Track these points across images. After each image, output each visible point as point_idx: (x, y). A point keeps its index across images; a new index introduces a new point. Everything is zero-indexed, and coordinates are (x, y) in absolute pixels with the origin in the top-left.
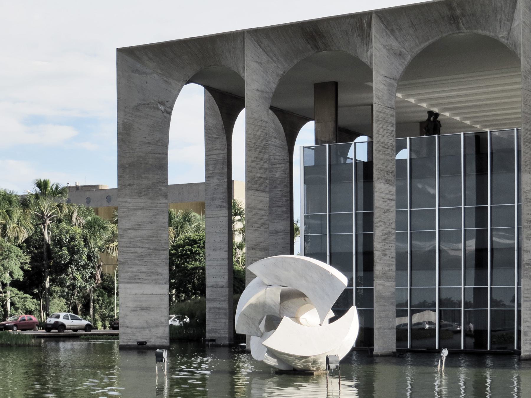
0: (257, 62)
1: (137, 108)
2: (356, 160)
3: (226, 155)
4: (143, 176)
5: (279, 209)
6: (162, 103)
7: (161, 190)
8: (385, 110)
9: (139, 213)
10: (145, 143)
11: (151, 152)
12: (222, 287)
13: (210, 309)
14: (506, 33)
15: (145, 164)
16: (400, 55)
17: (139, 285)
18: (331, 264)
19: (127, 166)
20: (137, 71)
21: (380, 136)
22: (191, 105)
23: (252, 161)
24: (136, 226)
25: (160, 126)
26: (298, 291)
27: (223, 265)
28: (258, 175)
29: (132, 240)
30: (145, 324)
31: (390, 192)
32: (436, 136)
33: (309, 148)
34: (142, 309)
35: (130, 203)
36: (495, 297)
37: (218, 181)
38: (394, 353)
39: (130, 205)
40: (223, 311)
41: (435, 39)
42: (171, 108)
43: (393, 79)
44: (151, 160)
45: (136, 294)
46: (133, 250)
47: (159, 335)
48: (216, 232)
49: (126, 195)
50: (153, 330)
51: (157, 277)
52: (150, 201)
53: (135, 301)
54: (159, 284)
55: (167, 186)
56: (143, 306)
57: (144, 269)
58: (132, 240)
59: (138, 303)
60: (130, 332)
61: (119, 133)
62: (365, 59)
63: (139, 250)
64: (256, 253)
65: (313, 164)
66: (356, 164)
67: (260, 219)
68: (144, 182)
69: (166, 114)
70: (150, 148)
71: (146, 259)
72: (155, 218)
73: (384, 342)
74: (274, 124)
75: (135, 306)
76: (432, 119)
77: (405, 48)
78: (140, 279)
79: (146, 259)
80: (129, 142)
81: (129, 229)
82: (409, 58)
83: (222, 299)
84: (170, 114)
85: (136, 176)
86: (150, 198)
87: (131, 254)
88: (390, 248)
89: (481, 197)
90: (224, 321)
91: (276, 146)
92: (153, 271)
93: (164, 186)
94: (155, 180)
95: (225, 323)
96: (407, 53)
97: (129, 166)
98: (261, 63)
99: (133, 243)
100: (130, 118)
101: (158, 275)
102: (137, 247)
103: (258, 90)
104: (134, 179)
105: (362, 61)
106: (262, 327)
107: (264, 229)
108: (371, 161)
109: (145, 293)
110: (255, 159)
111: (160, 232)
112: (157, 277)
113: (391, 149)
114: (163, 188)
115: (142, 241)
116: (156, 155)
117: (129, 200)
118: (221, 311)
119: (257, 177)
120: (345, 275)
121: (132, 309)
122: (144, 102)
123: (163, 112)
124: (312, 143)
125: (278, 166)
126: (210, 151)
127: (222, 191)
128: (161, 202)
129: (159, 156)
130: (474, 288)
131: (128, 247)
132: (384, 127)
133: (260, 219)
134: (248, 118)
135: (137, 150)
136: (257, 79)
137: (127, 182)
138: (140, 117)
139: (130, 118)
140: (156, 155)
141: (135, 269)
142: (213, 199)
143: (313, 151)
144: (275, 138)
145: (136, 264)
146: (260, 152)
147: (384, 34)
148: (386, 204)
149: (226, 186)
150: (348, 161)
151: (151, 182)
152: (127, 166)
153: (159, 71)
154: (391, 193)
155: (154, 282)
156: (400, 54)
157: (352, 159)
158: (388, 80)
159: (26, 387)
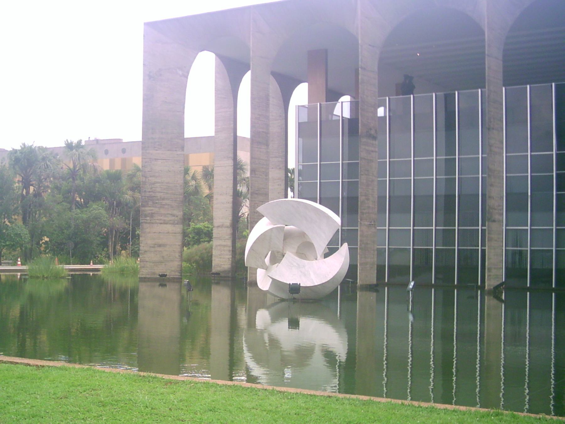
2: (342, 117)
13: (216, 246)
18: (320, 203)
22: (205, 68)
32: (412, 96)
33: (303, 106)
36: (438, 194)
38: (218, 283)
42: (188, 73)
55: (184, 139)
62: (308, 240)
65: (307, 121)
66: (343, 120)
73: (365, 276)
74: (274, 87)
76: (407, 82)
84: (187, 77)
89: (450, 149)
106: (267, 260)
108: (354, 117)
118: (225, 248)
120: (294, 89)
124: (305, 102)
130: (446, 159)
134: (253, 80)
143: (306, 110)
149: (232, 139)
150: (334, 118)
157: (339, 116)
159: (205, 169)
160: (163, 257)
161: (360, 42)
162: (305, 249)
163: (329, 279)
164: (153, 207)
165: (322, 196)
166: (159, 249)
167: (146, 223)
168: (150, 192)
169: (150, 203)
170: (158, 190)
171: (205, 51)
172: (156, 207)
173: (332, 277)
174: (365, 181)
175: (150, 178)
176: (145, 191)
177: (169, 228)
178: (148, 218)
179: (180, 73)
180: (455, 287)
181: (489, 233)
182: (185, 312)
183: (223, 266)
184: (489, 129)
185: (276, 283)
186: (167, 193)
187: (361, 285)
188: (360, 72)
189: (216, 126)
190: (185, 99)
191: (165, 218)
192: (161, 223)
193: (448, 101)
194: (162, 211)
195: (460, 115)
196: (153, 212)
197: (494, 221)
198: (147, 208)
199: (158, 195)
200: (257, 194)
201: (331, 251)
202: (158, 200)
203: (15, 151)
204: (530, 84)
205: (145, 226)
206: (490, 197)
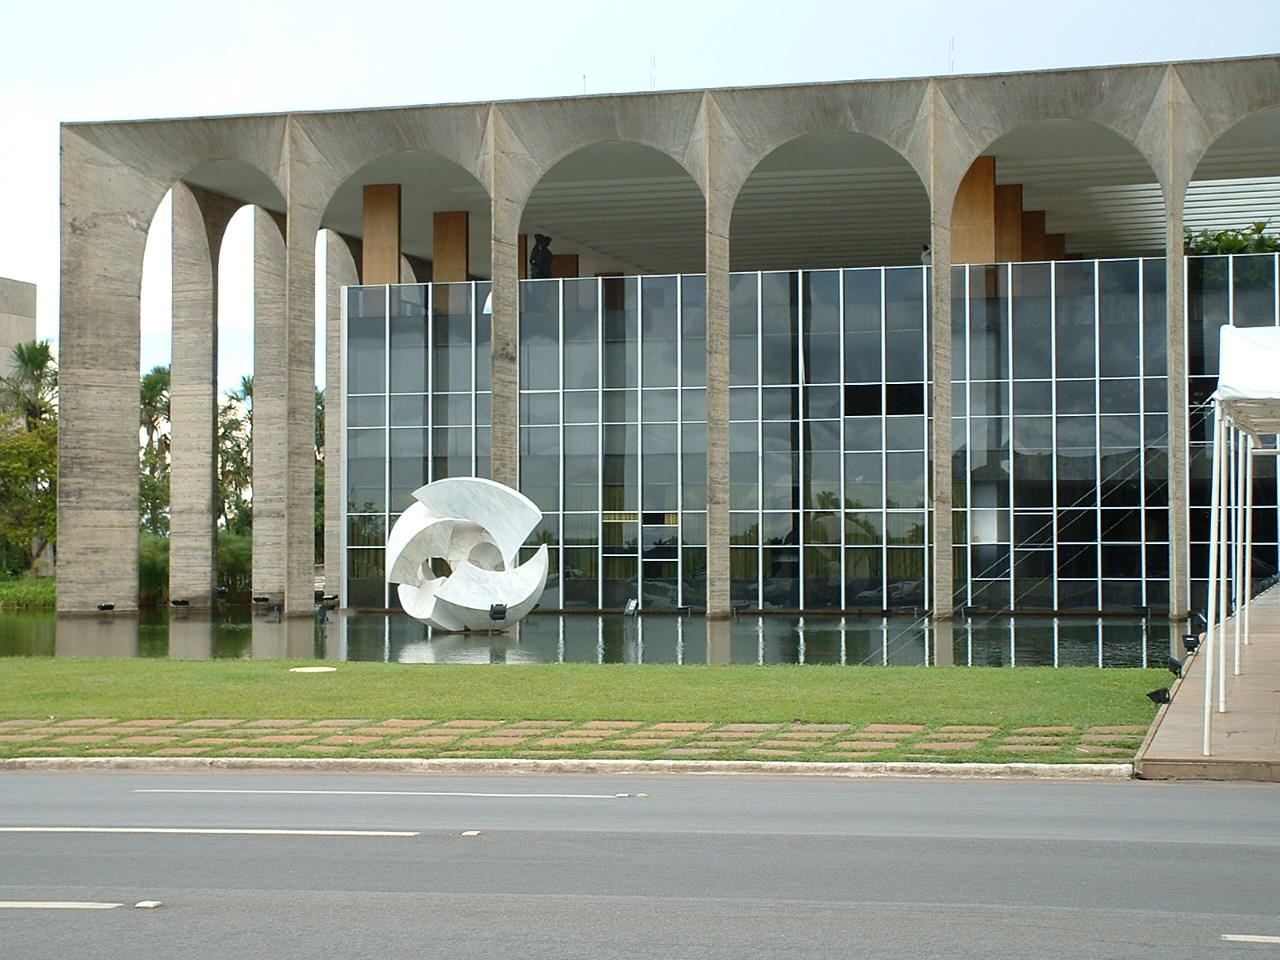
3: (211, 292)
5: (272, 379)
6: (134, 215)
12: (202, 512)
13: (178, 549)
14: (682, 147)
26: (476, 524)
27: (203, 476)
37: (195, 335)
40: (202, 553)
48: (190, 420)
60: (75, 590)
69: (138, 232)
75: (85, 546)
77: (534, 158)
83: (201, 532)
84: (146, 231)
90: (202, 569)
91: (269, 273)
93: (133, 349)
95: (205, 573)
105: (466, 171)
125: (272, 306)
126: (180, 284)
127: (202, 352)
135: (92, 289)
136: (307, 178)
140: (122, 298)
142: (187, 364)
144: (268, 259)
160: (102, 573)
161: (492, 195)
162: (486, 553)
163: (524, 599)
164: (82, 477)
165: (393, 456)
166: (92, 557)
167: (69, 508)
168: (75, 448)
169: (76, 470)
170: (92, 444)
171: (791, 530)
172: (87, 477)
173: (529, 595)
174: (500, 435)
175: (75, 423)
176: (66, 448)
177: (113, 516)
178: (73, 499)
179: (134, 222)
180: (1010, 614)
181: (711, 523)
182: (205, 379)
183: (193, 588)
184: (710, 353)
185: (442, 605)
186: (109, 451)
187: (289, 612)
188: (493, 246)
189: (173, 316)
190: (141, 271)
191: (106, 499)
192: (98, 509)
193: (529, 453)
194: (100, 485)
195: (393, 448)
196: (82, 486)
197: (718, 503)
198: (69, 480)
199: (92, 454)
200: (296, 454)
201: (525, 555)
202: (91, 463)
203: (435, 653)
204: (802, 268)
205: (68, 513)
206: (711, 463)
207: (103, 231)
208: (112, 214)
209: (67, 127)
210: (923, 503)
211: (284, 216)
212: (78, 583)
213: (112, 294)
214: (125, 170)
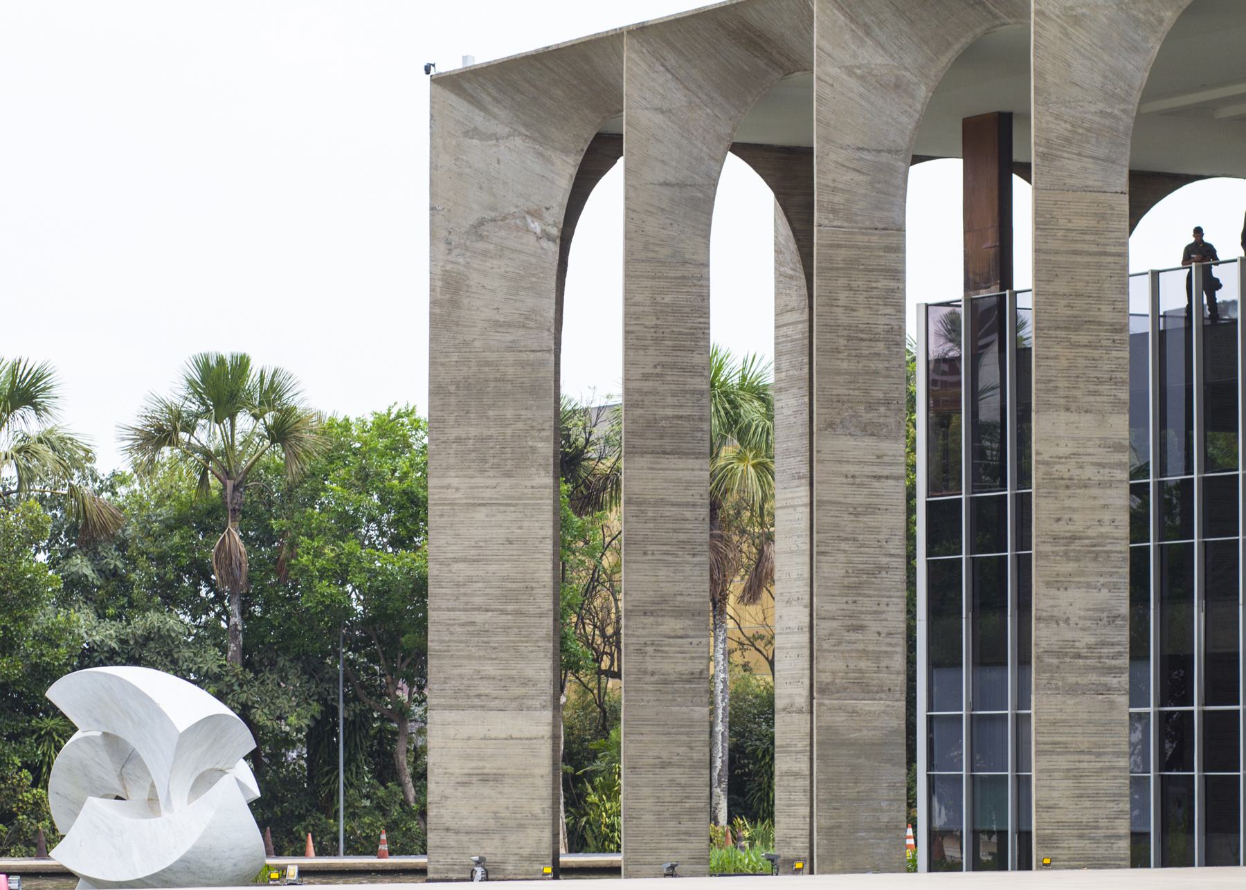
0: (661, 111)
1: (477, 230)
4: (491, 413)
6: (536, 214)
7: (534, 450)
8: (859, 238)
9: (480, 515)
10: (497, 325)
11: (512, 348)
15: (496, 380)
16: (897, 86)
17: (480, 713)
19: (452, 388)
20: (473, 133)
21: (839, 311)
23: (646, 377)
24: (472, 552)
25: (533, 275)
28: (669, 412)
29: (462, 590)
30: (492, 822)
31: (878, 457)
34: (485, 779)
35: (457, 489)
39: (457, 495)
41: (963, 40)
43: (889, 151)
44: (510, 370)
45: (469, 739)
46: (462, 616)
47: (526, 852)
49: (448, 468)
50: (512, 838)
51: (522, 691)
52: (508, 482)
53: (468, 757)
54: (528, 709)
56: (486, 771)
57: (490, 669)
58: (462, 590)
59: (474, 764)
60: (453, 844)
61: (434, 303)
63: (480, 617)
64: (658, 624)
67: (675, 530)
68: (492, 432)
70: (509, 338)
71: (495, 640)
72: (520, 528)
75: (466, 771)
77: (906, 69)
78: (479, 696)
79: (495, 640)
80: (457, 324)
81: (456, 560)
82: (923, 92)
85: (472, 416)
86: (508, 475)
87: (459, 629)
88: (883, 607)
92: (514, 672)
94: (520, 425)
96: (915, 79)
97: (458, 387)
98: (670, 111)
99: (463, 599)
100: (461, 260)
101: (524, 684)
102: (475, 609)
103: (666, 184)
104: (470, 425)
107: (689, 558)
109: (493, 734)
110: (658, 370)
111: (532, 565)
112: (522, 691)
113: (886, 340)
114: (540, 445)
115: (488, 591)
116: (524, 356)
117: (455, 482)
119: (666, 418)
121: (459, 780)
122: (493, 214)
123: (539, 238)
128: (534, 483)
129: (532, 356)
131: (453, 610)
132: (854, 284)
133: (675, 530)
135: (477, 344)
137: (453, 433)
138: (485, 254)
139: (461, 260)
140: (524, 356)
141: (468, 669)
145: (469, 657)
146: (675, 348)
147: (847, 37)
148: (866, 491)
151: (509, 431)
152: (452, 388)
153: (523, 130)
154: (886, 459)
155: (515, 704)
156: (898, 86)
158: (667, 192)
179: (536, 226)
207: (491, 247)
208: (504, 219)
209: (454, 85)
210: (914, 860)
211: (805, 154)
212: (457, 832)
213: (510, 349)
214: (518, 141)
